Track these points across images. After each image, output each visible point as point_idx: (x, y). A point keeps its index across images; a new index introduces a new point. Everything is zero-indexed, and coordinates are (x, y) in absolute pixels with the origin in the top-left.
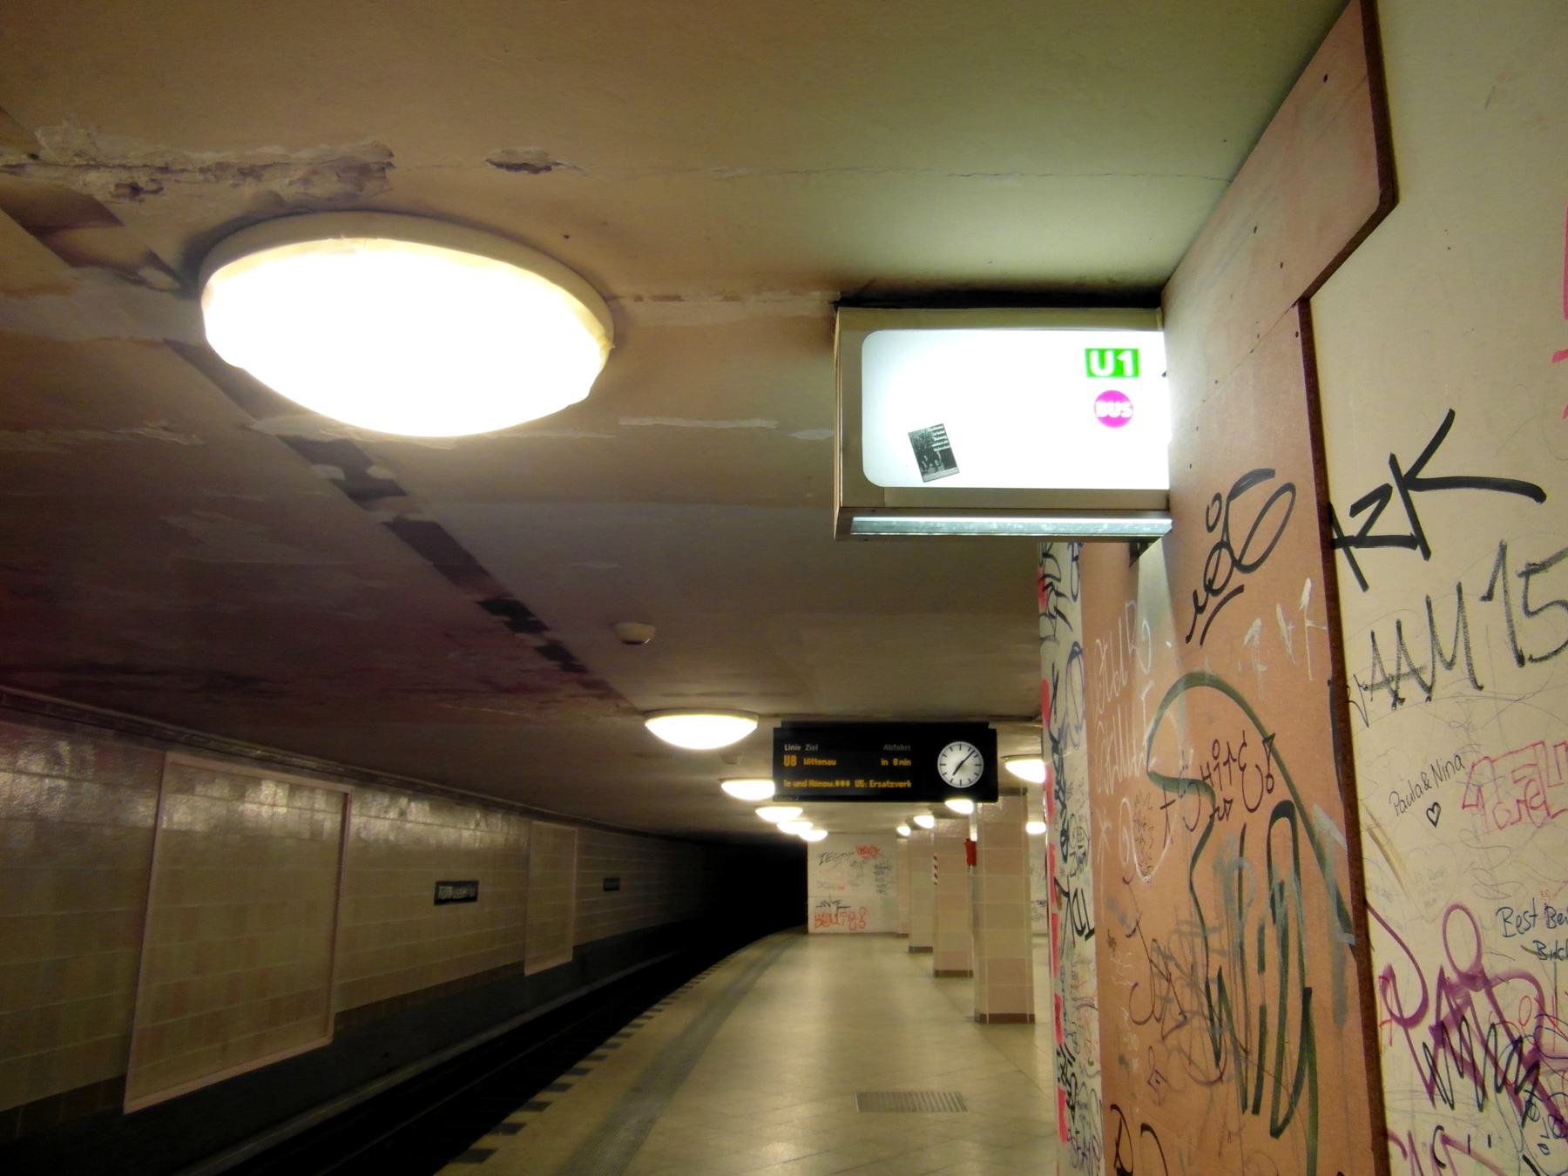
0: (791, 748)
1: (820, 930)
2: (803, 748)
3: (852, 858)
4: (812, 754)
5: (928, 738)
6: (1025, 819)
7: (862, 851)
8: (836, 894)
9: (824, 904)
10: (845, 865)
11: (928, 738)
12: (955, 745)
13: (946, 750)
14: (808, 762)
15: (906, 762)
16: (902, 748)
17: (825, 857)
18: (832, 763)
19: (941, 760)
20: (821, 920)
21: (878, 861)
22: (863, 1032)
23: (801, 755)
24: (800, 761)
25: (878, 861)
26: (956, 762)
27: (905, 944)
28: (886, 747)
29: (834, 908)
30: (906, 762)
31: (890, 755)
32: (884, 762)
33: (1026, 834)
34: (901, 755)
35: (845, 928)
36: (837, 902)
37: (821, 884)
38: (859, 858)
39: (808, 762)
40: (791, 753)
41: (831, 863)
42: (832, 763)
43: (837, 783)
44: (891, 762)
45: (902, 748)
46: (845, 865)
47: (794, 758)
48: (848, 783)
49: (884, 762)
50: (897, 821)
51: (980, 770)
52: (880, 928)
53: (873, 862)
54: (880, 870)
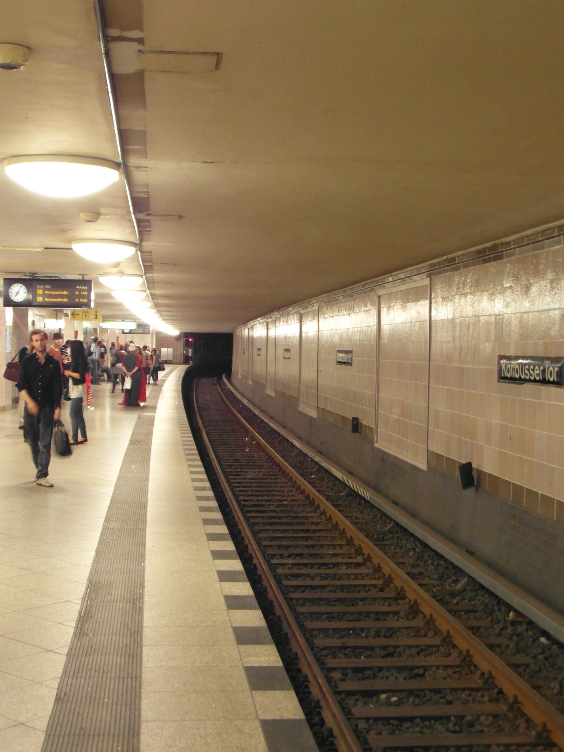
0: (40, 287)
4: (48, 290)
16: (84, 288)
18: (65, 293)
23: (44, 289)
32: (77, 293)
40: (40, 289)
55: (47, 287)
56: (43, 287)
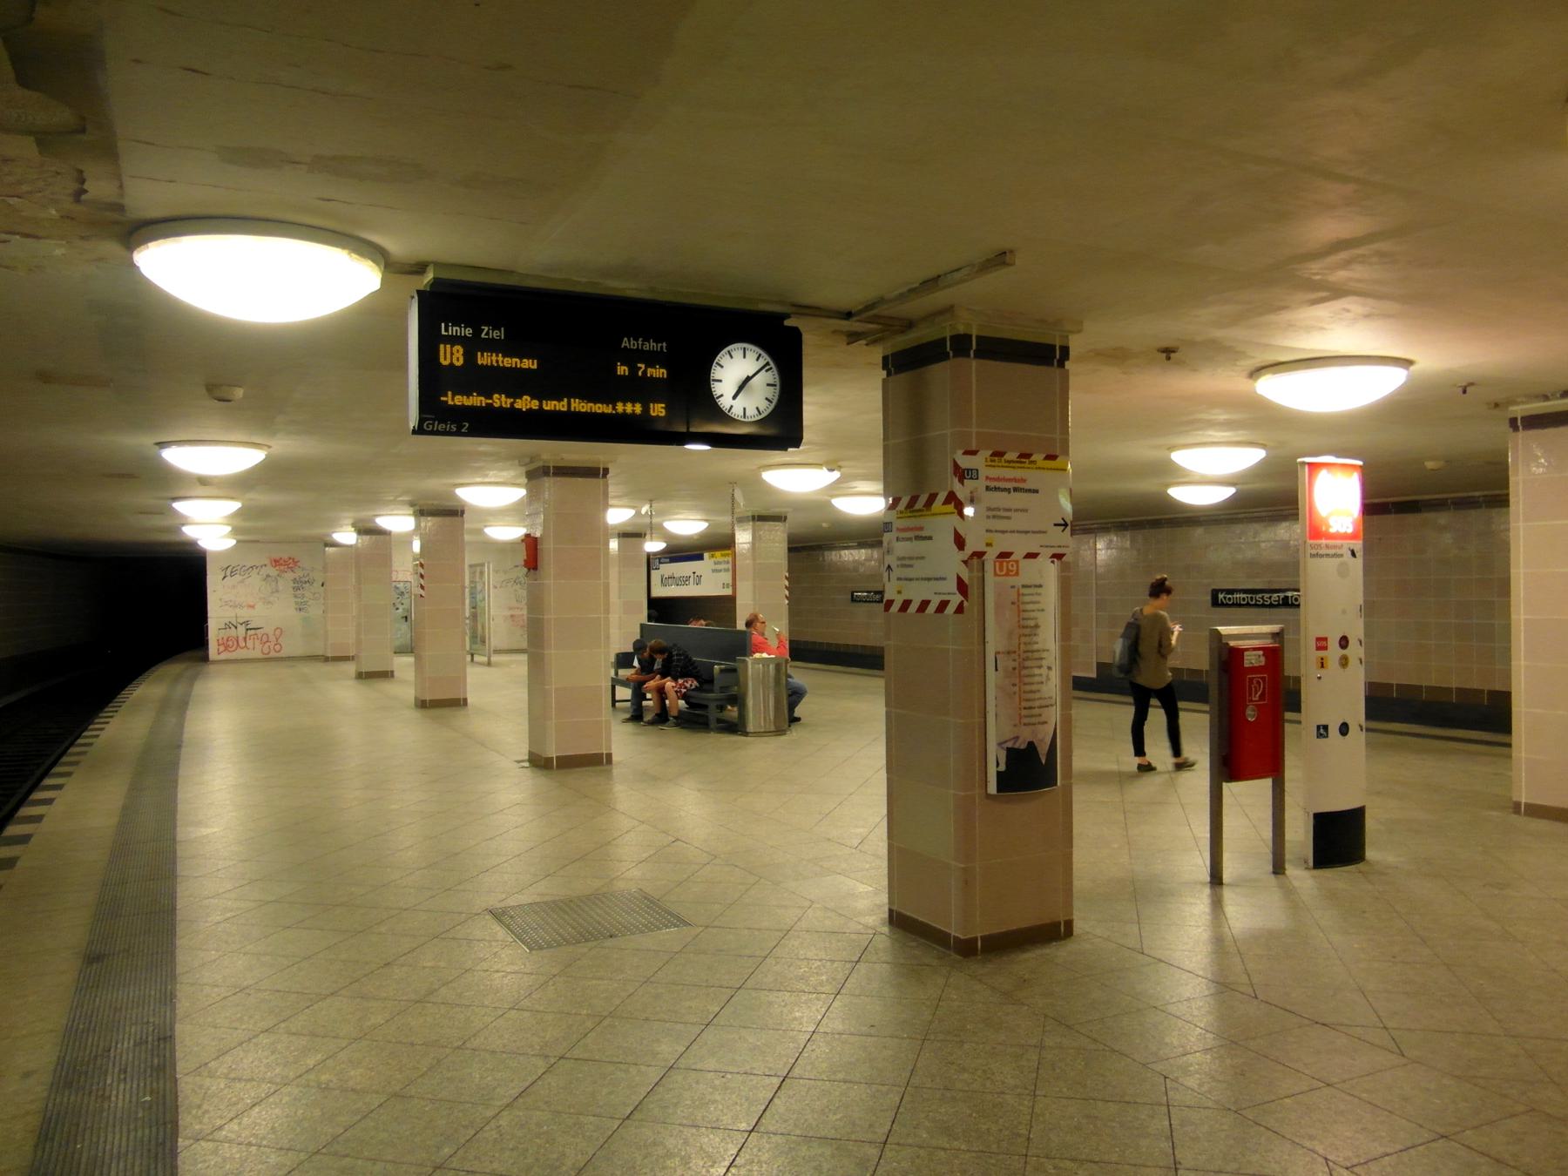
0: (454, 330)
1: (223, 656)
2: (477, 332)
3: (264, 571)
4: (491, 346)
5: (696, 332)
6: (607, 506)
7: (276, 562)
8: (244, 614)
9: (228, 626)
10: (255, 579)
11: (696, 332)
12: (737, 348)
13: (723, 357)
14: (484, 359)
15: (659, 372)
16: (651, 346)
17: (229, 571)
18: (529, 364)
19: (716, 373)
20: (225, 645)
21: (299, 573)
22: (290, 754)
23: (472, 346)
24: (470, 356)
25: (299, 573)
26: (740, 381)
27: (351, 668)
28: (625, 343)
29: (241, 630)
30: (659, 372)
31: (631, 358)
32: (622, 370)
33: (605, 524)
34: (652, 359)
35: (257, 654)
36: (246, 623)
37: (224, 603)
38: (273, 572)
39: (484, 359)
40: (453, 340)
41: (238, 578)
42: (529, 364)
43: (620, 407)
44: (633, 370)
45: (651, 346)
46: (255, 579)
47: (459, 351)
48: (638, 409)
49: (622, 370)
50: (334, 524)
51: (773, 394)
52: (300, 652)
53: (290, 575)
54: (299, 585)
55: (486, 332)
56: (468, 332)
